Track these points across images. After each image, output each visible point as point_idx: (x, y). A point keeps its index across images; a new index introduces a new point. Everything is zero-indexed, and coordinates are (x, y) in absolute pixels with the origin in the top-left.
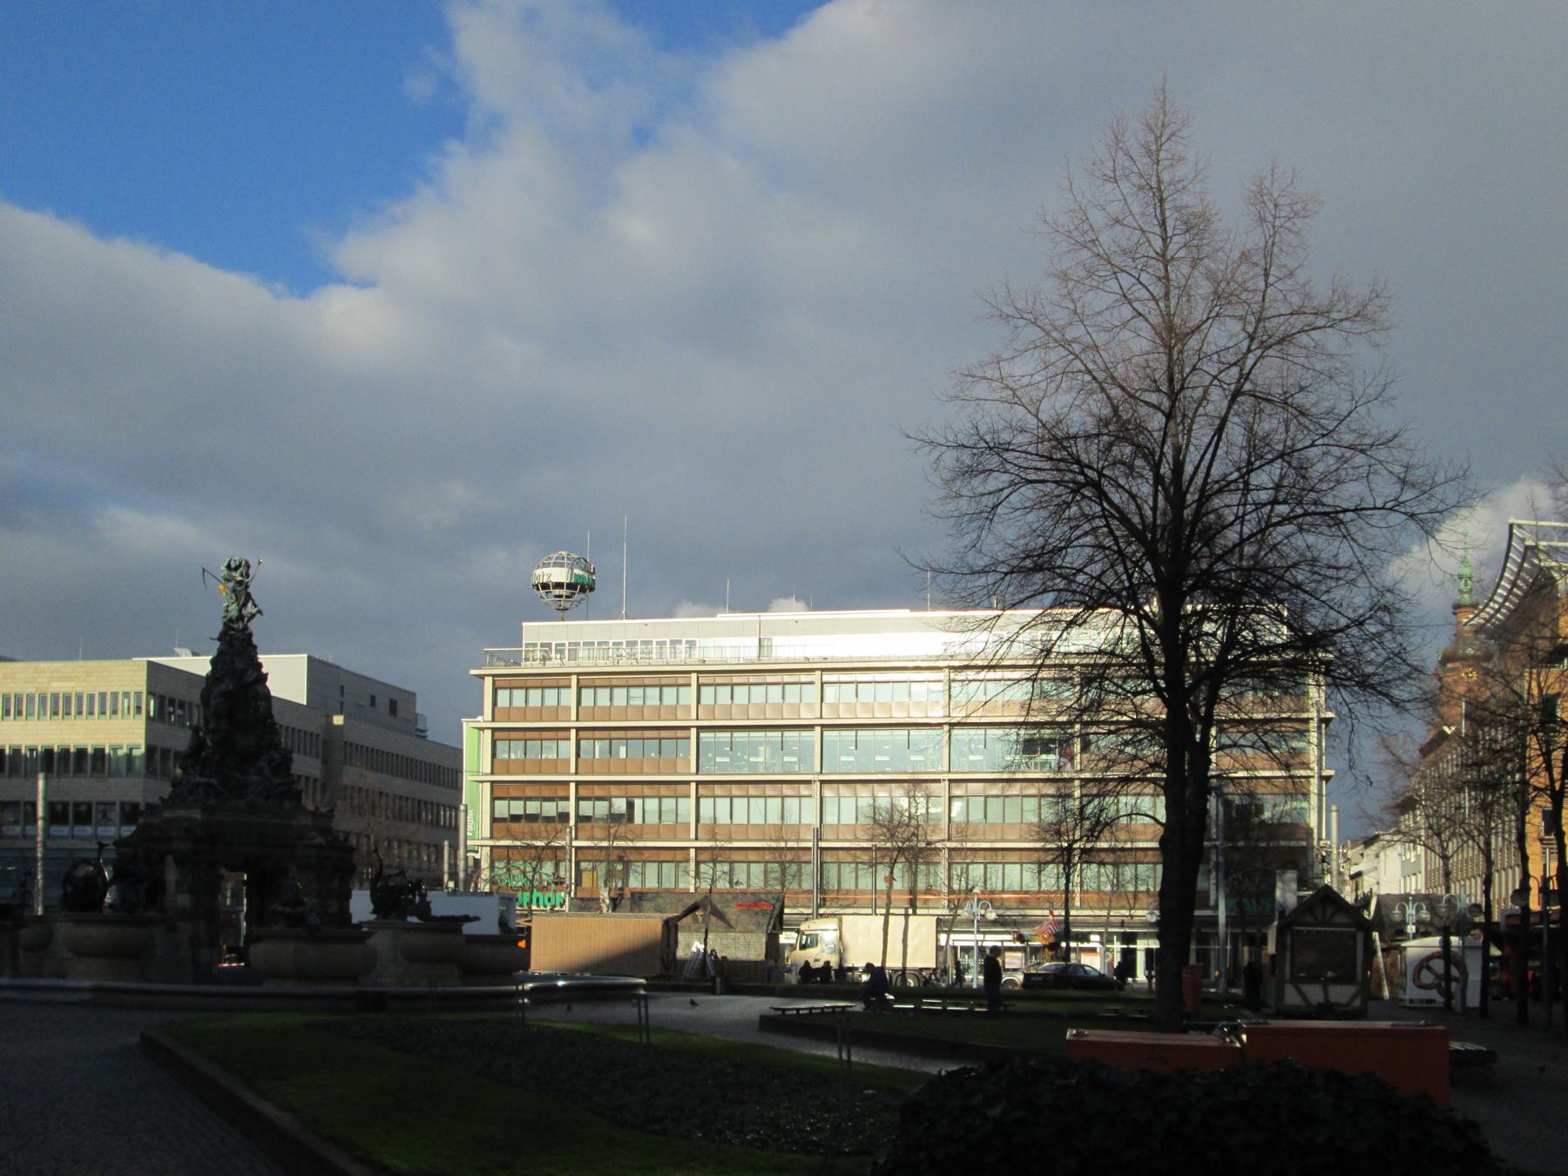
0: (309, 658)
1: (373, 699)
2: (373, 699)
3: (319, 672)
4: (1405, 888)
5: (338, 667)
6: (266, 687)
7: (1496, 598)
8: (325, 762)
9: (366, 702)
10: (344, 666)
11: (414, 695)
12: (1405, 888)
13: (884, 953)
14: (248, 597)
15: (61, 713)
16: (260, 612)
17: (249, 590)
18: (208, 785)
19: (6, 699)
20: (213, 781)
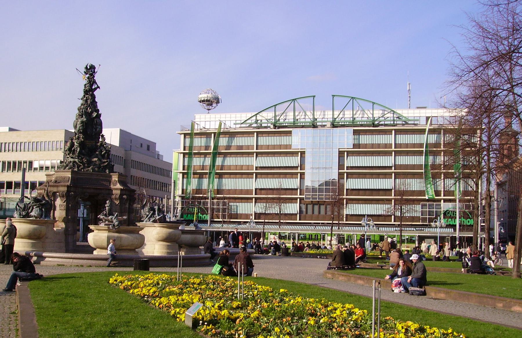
0: (121, 130)
1: (142, 145)
2: (142, 145)
3: (124, 134)
4: (436, 189)
5: (130, 133)
6: (100, 119)
7: (413, 230)
8: (124, 167)
9: (139, 146)
10: (132, 133)
11: (156, 143)
12: (436, 189)
13: (301, 107)
14: (95, 82)
15: (29, 188)
16: (98, 87)
17: (94, 79)
18: (74, 162)
19: (4, 163)
20: (76, 160)
